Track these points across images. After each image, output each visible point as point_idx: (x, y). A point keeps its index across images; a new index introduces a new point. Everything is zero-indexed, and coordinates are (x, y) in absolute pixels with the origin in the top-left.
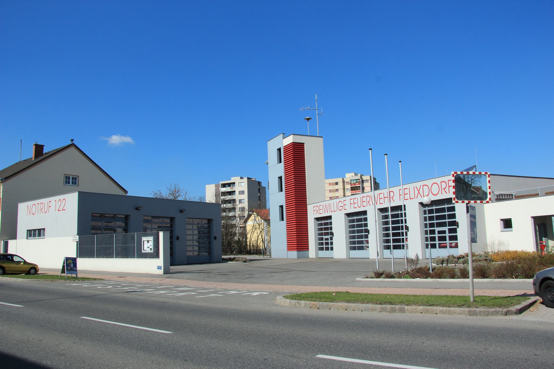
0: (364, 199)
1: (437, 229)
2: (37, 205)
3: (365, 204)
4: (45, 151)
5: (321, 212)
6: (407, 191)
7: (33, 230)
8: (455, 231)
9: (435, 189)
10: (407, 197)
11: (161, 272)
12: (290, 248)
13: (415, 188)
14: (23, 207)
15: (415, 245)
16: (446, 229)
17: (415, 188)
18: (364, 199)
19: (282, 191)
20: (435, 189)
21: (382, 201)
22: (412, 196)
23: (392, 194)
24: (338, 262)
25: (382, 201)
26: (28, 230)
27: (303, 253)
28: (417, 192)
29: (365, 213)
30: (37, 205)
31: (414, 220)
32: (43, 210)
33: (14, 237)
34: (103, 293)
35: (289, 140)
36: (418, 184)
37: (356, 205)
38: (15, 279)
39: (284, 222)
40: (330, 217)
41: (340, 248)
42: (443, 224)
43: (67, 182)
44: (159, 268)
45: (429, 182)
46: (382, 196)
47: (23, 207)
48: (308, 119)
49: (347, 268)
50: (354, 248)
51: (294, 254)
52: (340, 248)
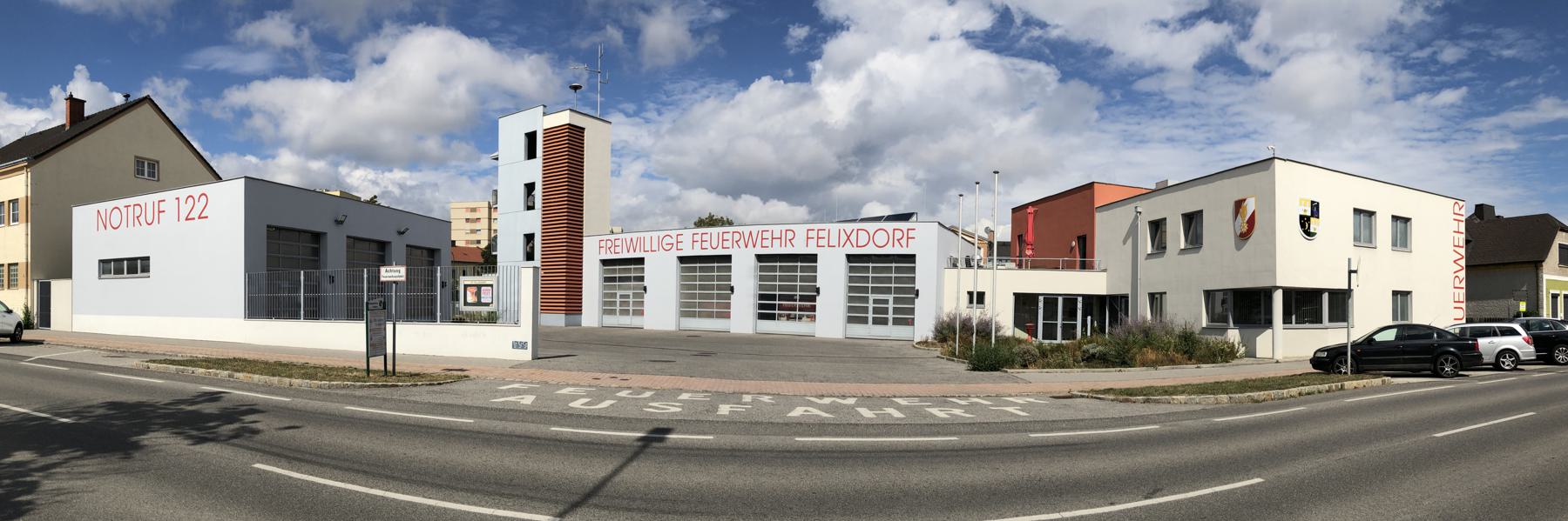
1: (872, 297)
2: (124, 210)
3: (726, 244)
4: (88, 112)
6: (705, 237)
7: (115, 260)
10: (821, 242)
11: (526, 355)
14: (84, 217)
15: (830, 319)
19: (530, 208)
20: (881, 238)
22: (834, 241)
23: (790, 235)
26: (101, 261)
27: (573, 318)
28: (844, 238)
29: (728, 258)
30: (124, 210)
31: (832, 279)
32: (142, 219)
33: (66, 273)
34: (144, 399)
37: (705, 245)
40: (641, 261)
42: (888, 291)
43: (140, 172)
44: (519, 345)
47: (84, 217)
52: (661, 309)
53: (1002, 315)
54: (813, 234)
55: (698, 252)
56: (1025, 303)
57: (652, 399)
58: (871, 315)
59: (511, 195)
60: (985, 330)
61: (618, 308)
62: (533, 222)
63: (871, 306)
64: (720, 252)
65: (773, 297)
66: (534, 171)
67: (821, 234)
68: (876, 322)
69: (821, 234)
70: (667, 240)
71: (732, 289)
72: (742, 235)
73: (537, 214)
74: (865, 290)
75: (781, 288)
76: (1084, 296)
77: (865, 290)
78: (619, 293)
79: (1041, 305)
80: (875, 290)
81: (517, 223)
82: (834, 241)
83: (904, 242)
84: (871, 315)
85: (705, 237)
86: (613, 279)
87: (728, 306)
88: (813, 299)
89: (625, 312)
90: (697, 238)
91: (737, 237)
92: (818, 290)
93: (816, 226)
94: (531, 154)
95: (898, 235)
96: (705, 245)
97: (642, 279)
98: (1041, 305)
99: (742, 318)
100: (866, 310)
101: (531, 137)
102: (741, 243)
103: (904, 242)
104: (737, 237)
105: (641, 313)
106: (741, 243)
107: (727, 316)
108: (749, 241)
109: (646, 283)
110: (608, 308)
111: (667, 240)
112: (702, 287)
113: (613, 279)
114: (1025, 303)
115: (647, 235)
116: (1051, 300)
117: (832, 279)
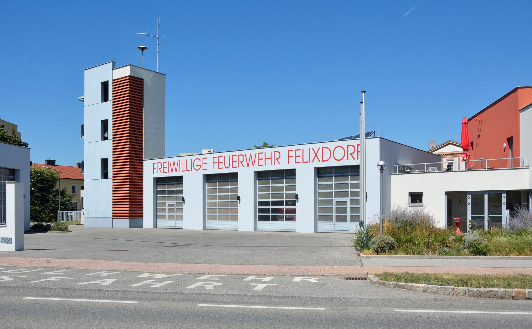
0: (235, 158)
1: (335, 200)
3: (235, 164)
5: (166, 170)
6: (299, 153)
8: (357, 202)
9: (339, 154)
10: (299, 159)
11: (11, 247)
12: (116, 215)
13: (311, 150)
15: (305, 219)
16: (348, 199)
17: (311, 150)
18: (235, 158)
19: (106, 138)
20: (339, 154)
21: (261, 162)
22: (306, 159)
24: (245, 237)
25: (261, 162)
27: (136, 220)
28: (313, 155)
29: (178, 180)
35: (125, 72)
36: (316, 147)
37: (221, 165)
38: (352, 271)
39: (109, 182)
41: (192, 216)
42: (346, 194)
45: (332, 145)
46: (261, 156)
48: (143, 49)
49: (203, 240)
50: (262, 218)
51: (124, 223)
52: (192, 216)
53: (436, 212)
54: (292, 154)
55: (216, 171)
56: (455, 200)
57: (43, 271)
58: (334, 214)
59: (93, 129)
60: (424, 223)
61: (349, 214)
62: (106, 149)
63: (334, 206)
64: (231, 170)
65: (267, 203)
66: (106, 111)
67: (298, 153)
68: (339, 219)
69: (298, 153)
70: (197, 162)
71: (239, 198)
72: (244, 156)
73: (109, 144)
74: (330, 194)
75: (274, 196)
76: (508, 192)
77: (330, 194)
78: (168, 202)
79: (469, 201)
80: (338, 194)
81: (97, 149)
82: (306, 159)
83: (355, 155)
84: (334, 214)
85: (299, 153)
86: (163, 192)
87: (236, 211)
88: (294, 203)
89: (171, 217)
90: (216, 160)
91: (241, 158)
92: (296, 197)
93: (294, 148)
94: (105, 98)
95: (351, 150)
96: (221, 165)
97: (181, 192)
98: (469, 201)
99: (246, 219)
100: (331, 210)
101: (105, 85)
102: (245, 163)
103: (355, 155)
104: (241, 158)
105: (180, 217)
106: (245, 163)
107: (236, 218)
108: (250, 161)
109: (184, 195)
110: (322, 215)
111: (197, 162)
112: (221, 197)
113: (163, 192)
114: (455, 200)
115: (184, 159)
116: (478, 196)
117: (305, 185)
